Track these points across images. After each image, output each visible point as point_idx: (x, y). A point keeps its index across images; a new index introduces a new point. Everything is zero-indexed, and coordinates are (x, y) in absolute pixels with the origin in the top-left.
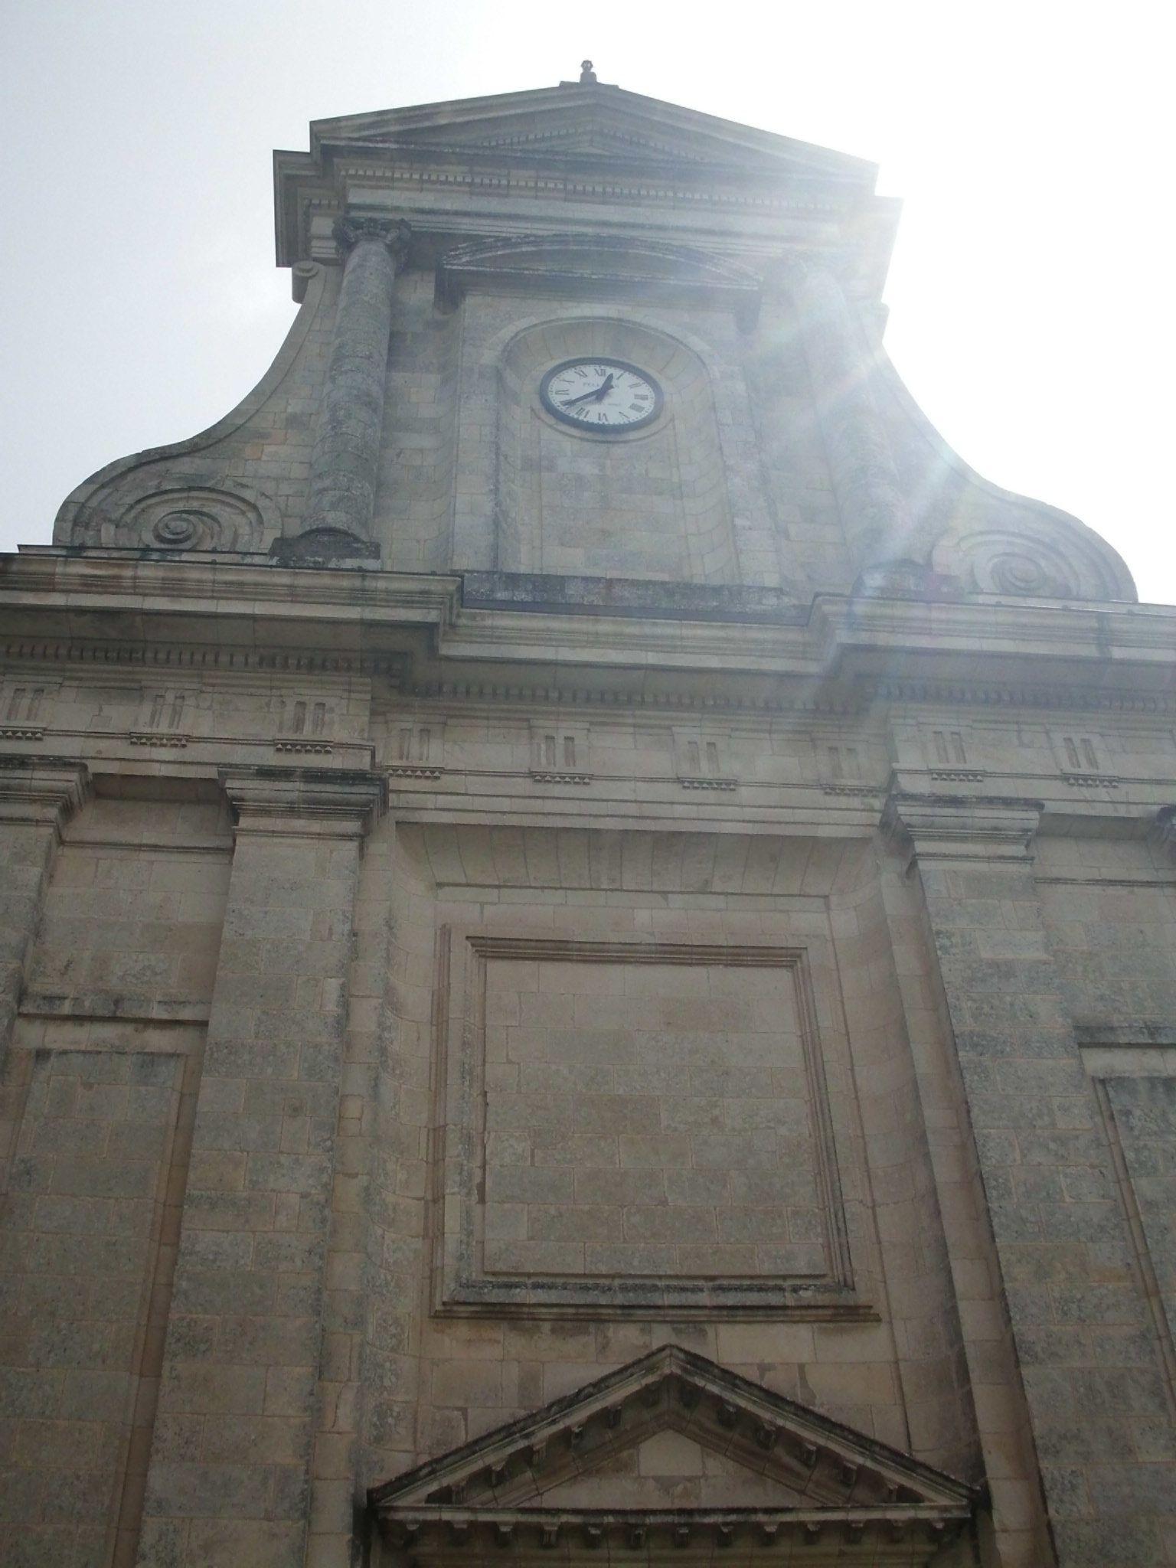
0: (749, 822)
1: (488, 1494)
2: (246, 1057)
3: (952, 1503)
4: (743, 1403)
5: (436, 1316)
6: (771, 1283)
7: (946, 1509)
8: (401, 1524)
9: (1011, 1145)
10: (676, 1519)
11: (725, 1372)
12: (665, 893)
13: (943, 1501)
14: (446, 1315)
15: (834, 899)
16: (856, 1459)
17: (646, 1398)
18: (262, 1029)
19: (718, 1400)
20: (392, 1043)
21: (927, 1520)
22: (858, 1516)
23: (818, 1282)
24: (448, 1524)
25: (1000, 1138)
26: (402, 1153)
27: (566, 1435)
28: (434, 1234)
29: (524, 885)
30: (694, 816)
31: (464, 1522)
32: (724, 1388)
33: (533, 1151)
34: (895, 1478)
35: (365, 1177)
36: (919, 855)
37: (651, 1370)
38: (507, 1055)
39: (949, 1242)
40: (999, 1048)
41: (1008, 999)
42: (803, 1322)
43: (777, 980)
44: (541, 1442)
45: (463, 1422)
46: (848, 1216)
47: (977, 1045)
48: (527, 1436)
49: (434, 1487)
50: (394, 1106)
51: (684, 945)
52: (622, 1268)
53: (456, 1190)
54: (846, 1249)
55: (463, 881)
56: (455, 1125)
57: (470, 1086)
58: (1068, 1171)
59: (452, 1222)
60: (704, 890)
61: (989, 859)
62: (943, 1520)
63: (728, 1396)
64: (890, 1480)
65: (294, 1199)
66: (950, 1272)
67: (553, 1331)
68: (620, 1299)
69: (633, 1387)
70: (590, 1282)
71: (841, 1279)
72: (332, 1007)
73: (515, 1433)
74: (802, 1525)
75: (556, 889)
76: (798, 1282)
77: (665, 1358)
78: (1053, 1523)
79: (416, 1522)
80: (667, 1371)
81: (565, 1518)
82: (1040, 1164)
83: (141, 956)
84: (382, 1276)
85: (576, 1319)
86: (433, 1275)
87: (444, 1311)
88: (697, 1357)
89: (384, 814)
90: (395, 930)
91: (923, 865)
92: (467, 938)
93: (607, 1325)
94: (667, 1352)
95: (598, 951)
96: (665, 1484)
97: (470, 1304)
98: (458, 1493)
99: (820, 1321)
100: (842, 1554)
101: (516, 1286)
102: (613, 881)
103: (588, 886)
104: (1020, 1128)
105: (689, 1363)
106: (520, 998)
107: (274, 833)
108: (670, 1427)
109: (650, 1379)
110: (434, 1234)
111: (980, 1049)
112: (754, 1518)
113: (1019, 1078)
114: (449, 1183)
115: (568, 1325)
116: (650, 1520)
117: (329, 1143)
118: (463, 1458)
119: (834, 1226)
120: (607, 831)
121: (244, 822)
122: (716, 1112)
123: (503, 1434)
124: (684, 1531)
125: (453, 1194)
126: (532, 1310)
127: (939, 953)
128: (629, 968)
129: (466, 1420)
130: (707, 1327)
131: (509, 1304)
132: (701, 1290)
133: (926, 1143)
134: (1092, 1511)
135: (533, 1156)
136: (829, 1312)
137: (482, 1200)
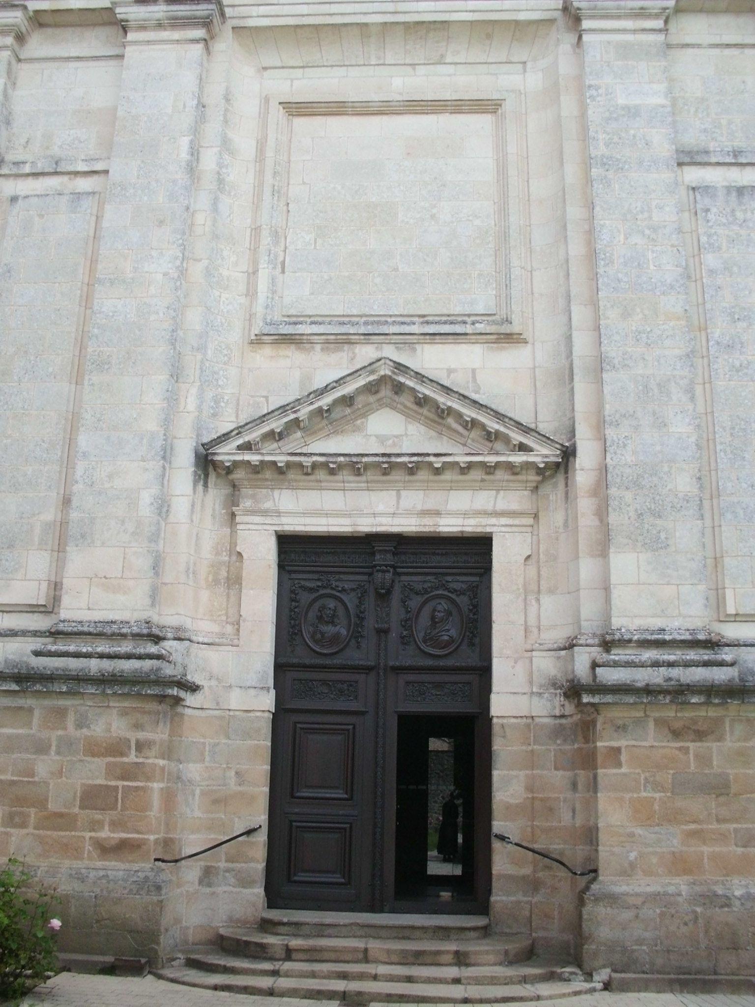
0: (470, 11)
1: (275, 445)
2: (132, 191)
3: (551, 453)
4: (427, 392)
5: (252, 343)
6: (460, 319)
7: (546, 456)
8: (222, 462)
9: (619, 231)
10: (381, 459)
11: (417, 373)
12: (413, 65)
13: (545, 451)
14: (258, 341)
15: (529, 65)
16: (493, 425)
17: (371, 388)
18: (142, 172)
19: (413, 390)
20: (228, 175)
21: (534, 462)
22: (492, 459)
23: (490, 318)
24: (248, 462)
25: (611, 227)
26: (234, 244)
27: (320, 411)
28: (251, 293)
29: (320, 64)
30: (433, 9)
31: (258, 460)
32: (417, 383)
33: (315, 240)
34: (517, 437)
35: (207, 261)
36: (584, 30)
37: (372, 372)
38: (303, 179)
39: (572, 295)
40: (621, 165)
41: (632, 132)
42: (477, 343)
43: (483, 122)
44: (304, 415)
45: (266, 404)
46: (512, 277)
47: (605, 164)
48: (295, 412)
49: (240, 442)
50: (230, 216)
51: (422, 101)
52: (367, 311)
53: (266, 266)
54: (509, 297)
55: (279, 64)
56: (267, 225)
57: (278, 200)
58: (655, 249)
59: (263, 286)
60: (441, 62)
61: (635, 31)
62: (544, 462)
63: (418, 387)
64: (514, 439)
65: (159, 277)
66: (570, 313)
67: (322, 349)
68: (362, 330)
69: (361, 382)
70: (346, 319)
71: (505, 316)
72: (184, 155)
73: (288, 410)
74: (457, 463)
75: (341, 66)
76: (478, 318)
77: (381, 365)
78: (608, 466)
79: (230, 461)
80: (382, 373)
81: (315, 458)
82: (636, 244)
83: (72, 131)
84: (219, 320)
85: (336, 342)
86: (251, 318)
87: (257, 340)
88: (399, 364)
89: (224, 22)
90: (231, 102)
91: (585, 38)
92: (280, 103)
93: (355, 345)
94: (382, 361)
95: (366, 107)
96: (381, 439)
97: (271, 335)
98: (255, 445)
99: (488, 343)
100: (483, 480)
101: (301, 323)
102: (379, 58)
103: (362, 63)
104: (626, 220)
105: (396, 368)
106: (313, 141)
107: (148, 42)
108: (387, 406)
109: (372, 378)
110: (251, 293)
111: (607, 167)
112: (427, 459)
113: (632, 186)
114: (262, 261)
115: (332, 346)
116: (365, 459)
117: (181, 241)
118: (257, 425)
119: (504, 283)
120: (373, 24)
121: (131, 36)
122: (434, 211)
123: (280, 411)
124: (386, 466)
125: (264, 268)
126: (309, 338)
127: (588, 101)
128: (385, 118)
129: (268, 403)
130: (417, 346)
131: (295, 334)
132: (414, 324)
133: (566, 230)
134: (634, 459)
135: (315, 243)
136: (495, 337)
137: (283, 272)
